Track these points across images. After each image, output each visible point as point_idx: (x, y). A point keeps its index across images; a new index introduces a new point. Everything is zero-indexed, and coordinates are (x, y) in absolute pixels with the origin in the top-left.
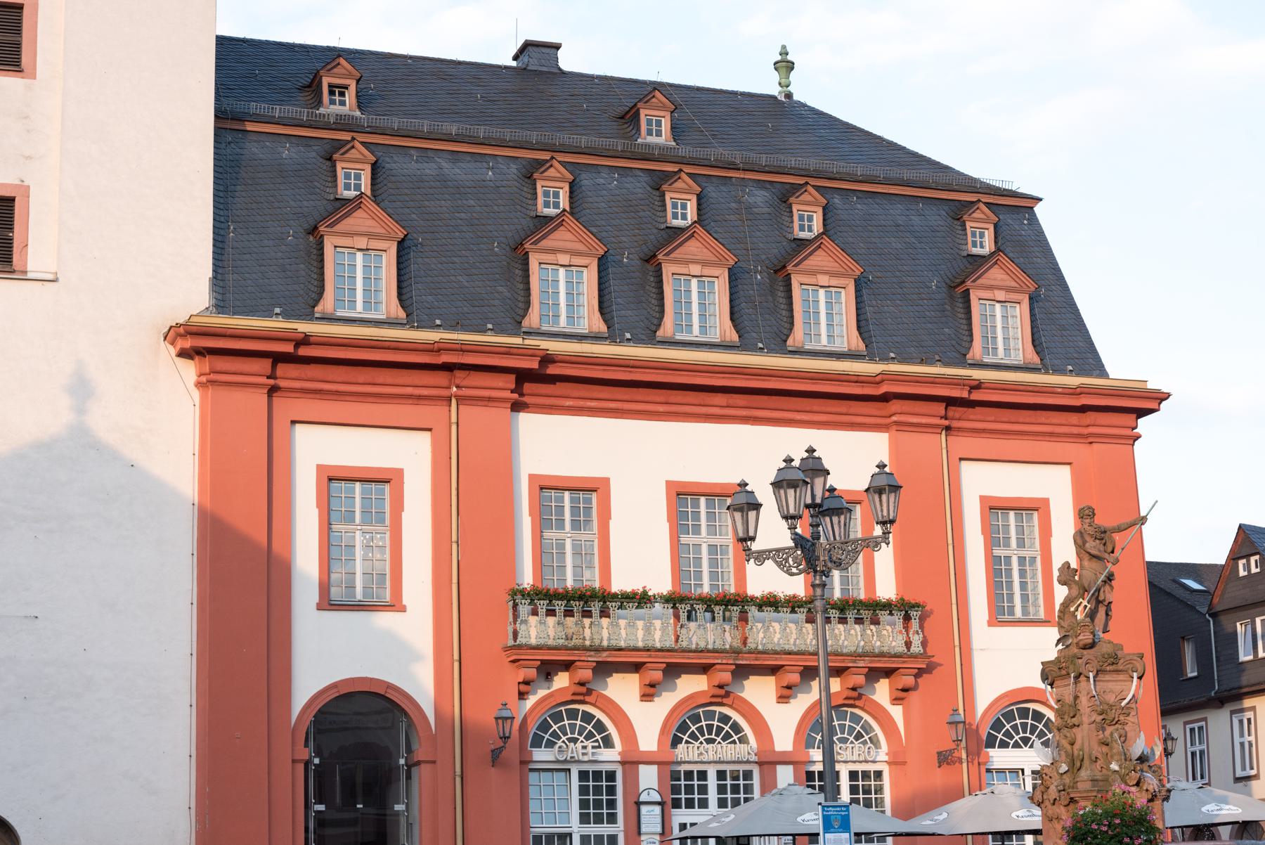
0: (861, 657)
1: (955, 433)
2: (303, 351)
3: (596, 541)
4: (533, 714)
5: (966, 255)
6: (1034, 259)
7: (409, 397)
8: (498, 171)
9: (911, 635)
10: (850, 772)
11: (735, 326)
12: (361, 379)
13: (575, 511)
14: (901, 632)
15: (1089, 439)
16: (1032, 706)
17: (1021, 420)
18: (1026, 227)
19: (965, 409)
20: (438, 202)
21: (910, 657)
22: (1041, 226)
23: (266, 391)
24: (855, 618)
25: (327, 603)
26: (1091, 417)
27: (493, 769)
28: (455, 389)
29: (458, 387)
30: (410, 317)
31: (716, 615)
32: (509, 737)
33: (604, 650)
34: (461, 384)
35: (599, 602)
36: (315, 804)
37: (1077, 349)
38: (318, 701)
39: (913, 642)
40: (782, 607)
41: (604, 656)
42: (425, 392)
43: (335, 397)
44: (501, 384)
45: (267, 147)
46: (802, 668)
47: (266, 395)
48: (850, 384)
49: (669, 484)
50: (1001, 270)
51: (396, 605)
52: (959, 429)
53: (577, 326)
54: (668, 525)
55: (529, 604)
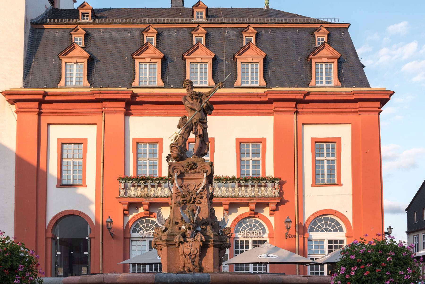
0: (252, 198)
1: (301, 114)
2: (307, 98)
3: (158, 160)
4: (131, 221)
5: (314, 47)
6: (345, 47)
7: (87, 113)
8: (132, 33)
9: (127, 190)
10: (253, 241)
11: (214, 80)
12: (71, 108)
13: (328, 150)
14: (123, 189)
15: (359, 113)
16: (330, 216)
17: (329, 107)
18: (343, 35)
19: (305, 104)
20: (108, 46)
21: (127, 198)
22: (349, 34)
23: (37, 113)
24: (258, 185)
25: (60, 184)
26: (359, 104)
27: (113, 240)
28: (103, 108)
29: (104, 108)
30: (91, 85)
31: (275, 184)
32: (111, 229)
33: (152, 197)
34: (105, 107)
35: (150, 181)
36: (87, 254)
37: (358, 79)
38: (57, 217)
39: (128, 192)
40: (222, 181)
41: (151, 200)
42: (93, 110)
43: (62, 114)
44: (119, 106)
45: (51, 33)
46: (229, 203)
47: (123, 115)
48: (255, 97)
49: (237, 139)
50: (326, 50)
51: (84, 185)
52: (302, 112)
53: (330, 84)
54: (311, 153)
55: (132, 183)
